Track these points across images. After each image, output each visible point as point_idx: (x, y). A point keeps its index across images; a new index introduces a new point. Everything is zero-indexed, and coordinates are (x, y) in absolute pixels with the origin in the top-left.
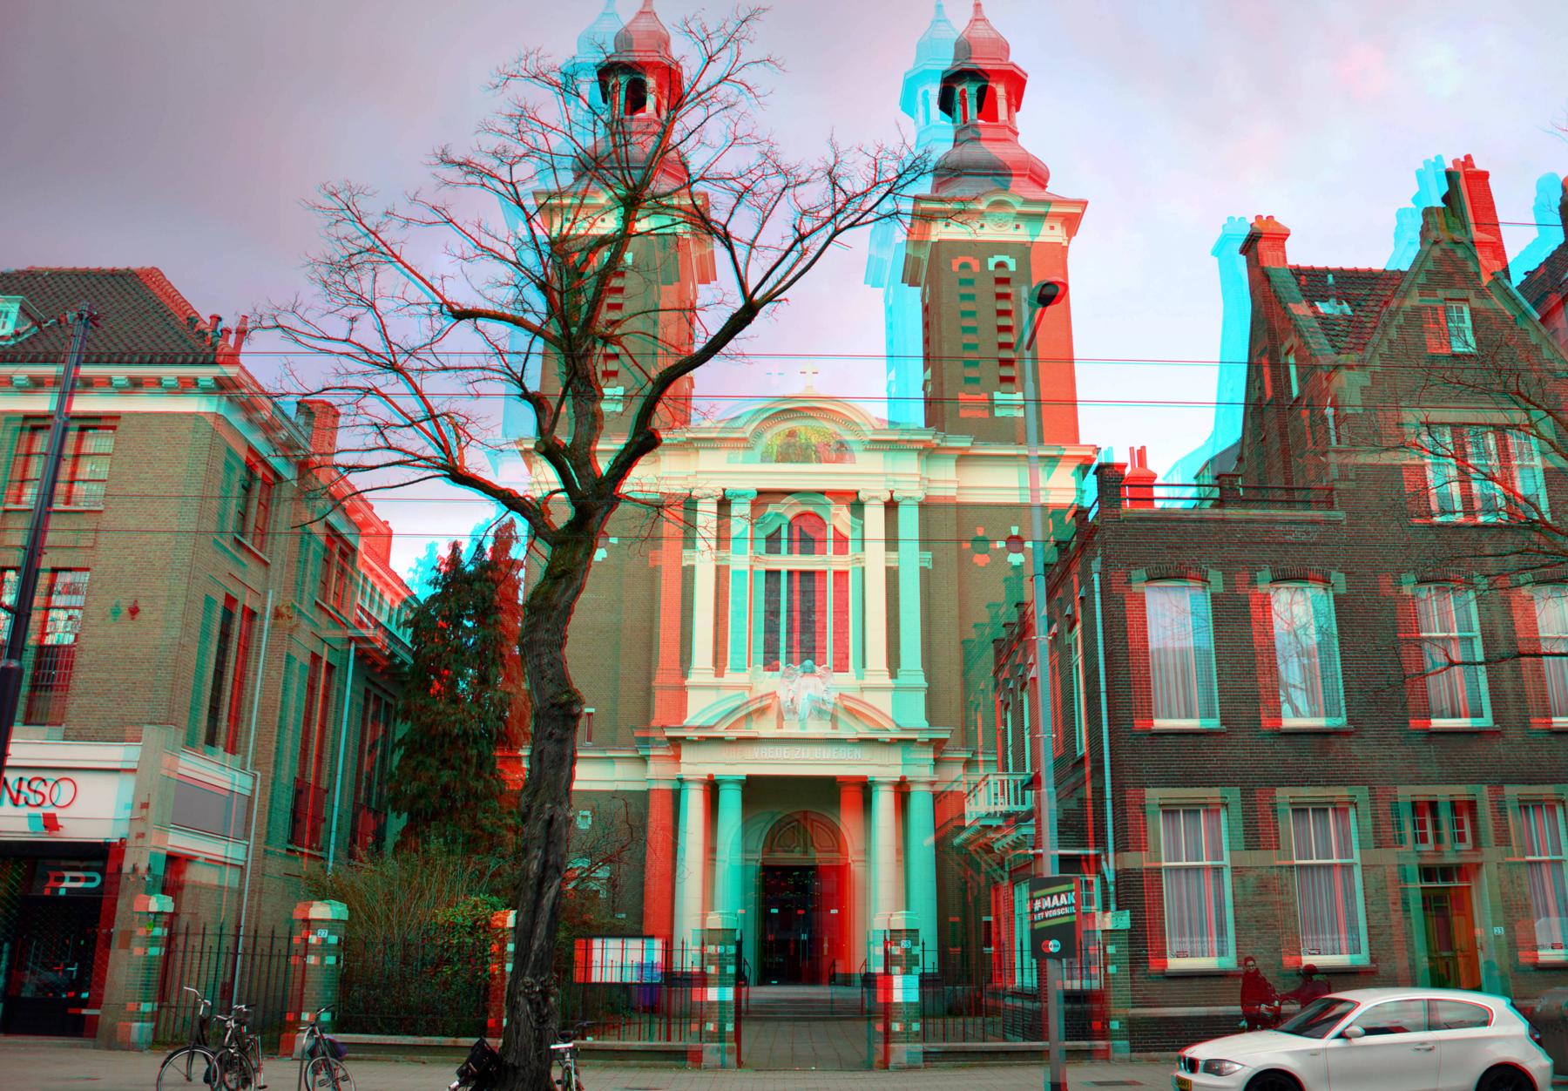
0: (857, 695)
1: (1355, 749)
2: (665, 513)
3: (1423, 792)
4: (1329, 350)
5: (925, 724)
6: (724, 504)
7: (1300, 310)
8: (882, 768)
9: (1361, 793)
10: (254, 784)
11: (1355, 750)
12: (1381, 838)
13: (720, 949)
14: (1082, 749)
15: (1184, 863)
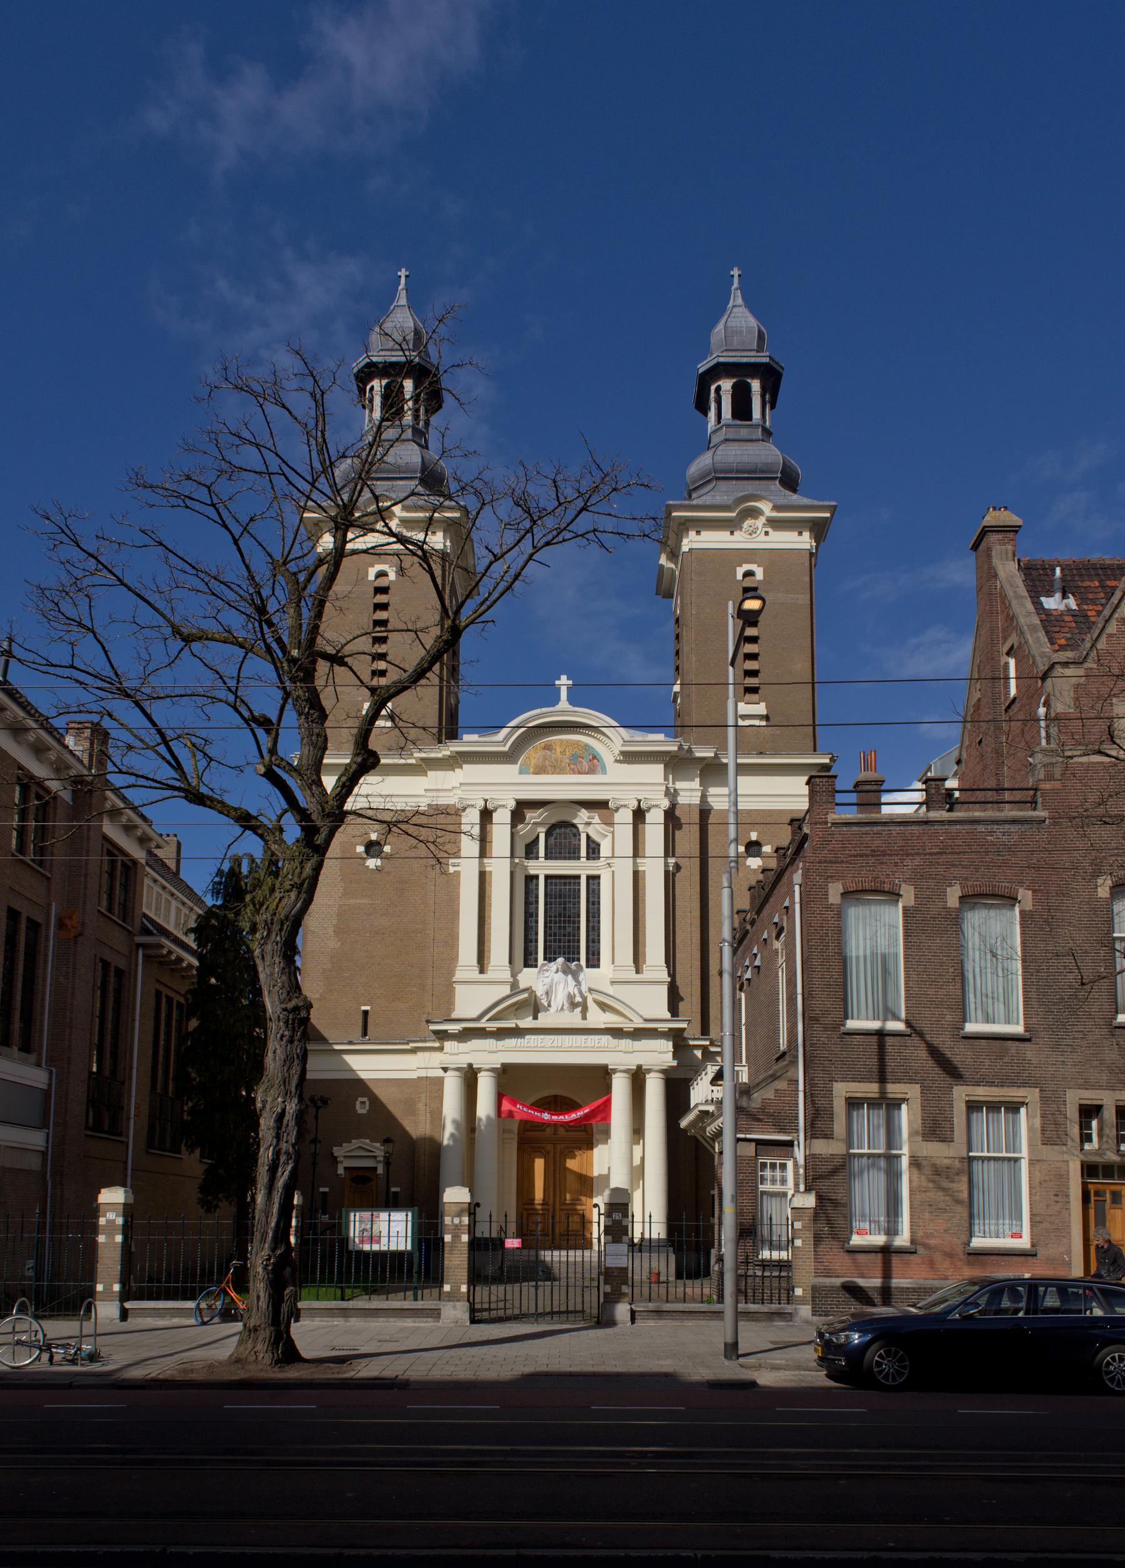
0: (610, 990)
1: (1029, 1051)
2: (394, 829)
3: (1090, 1096)
4: (1047, 648)
5: (668, 1015)
6: (486, 815)
7: (1023, 609)
8: (620, 1056)
9: (1032, 1095)
10: (50, 1079)
11: (1029, 1055)
12: (1050, 1133)
13: (456, 1221)
14: (783, 1045)
15: (866, 1151)
